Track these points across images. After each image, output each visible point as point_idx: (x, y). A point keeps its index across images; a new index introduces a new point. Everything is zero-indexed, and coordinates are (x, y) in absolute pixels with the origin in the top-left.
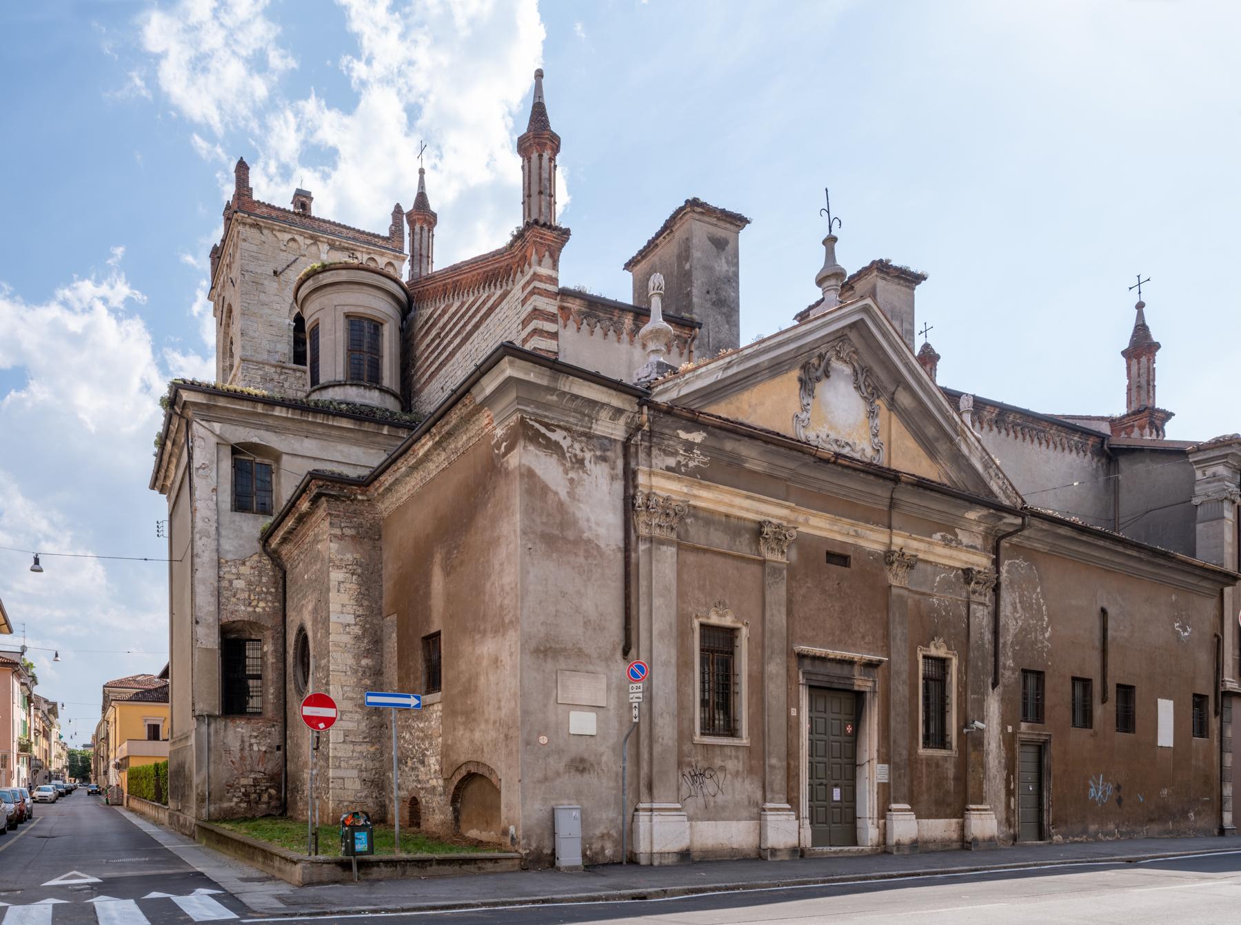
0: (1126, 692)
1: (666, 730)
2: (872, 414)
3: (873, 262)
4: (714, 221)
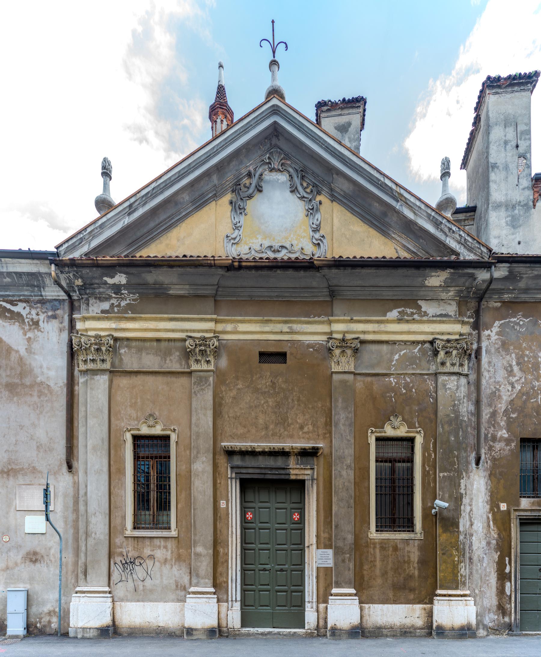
2: (312, 211)
3: (483, 84)
4: (339, 112)
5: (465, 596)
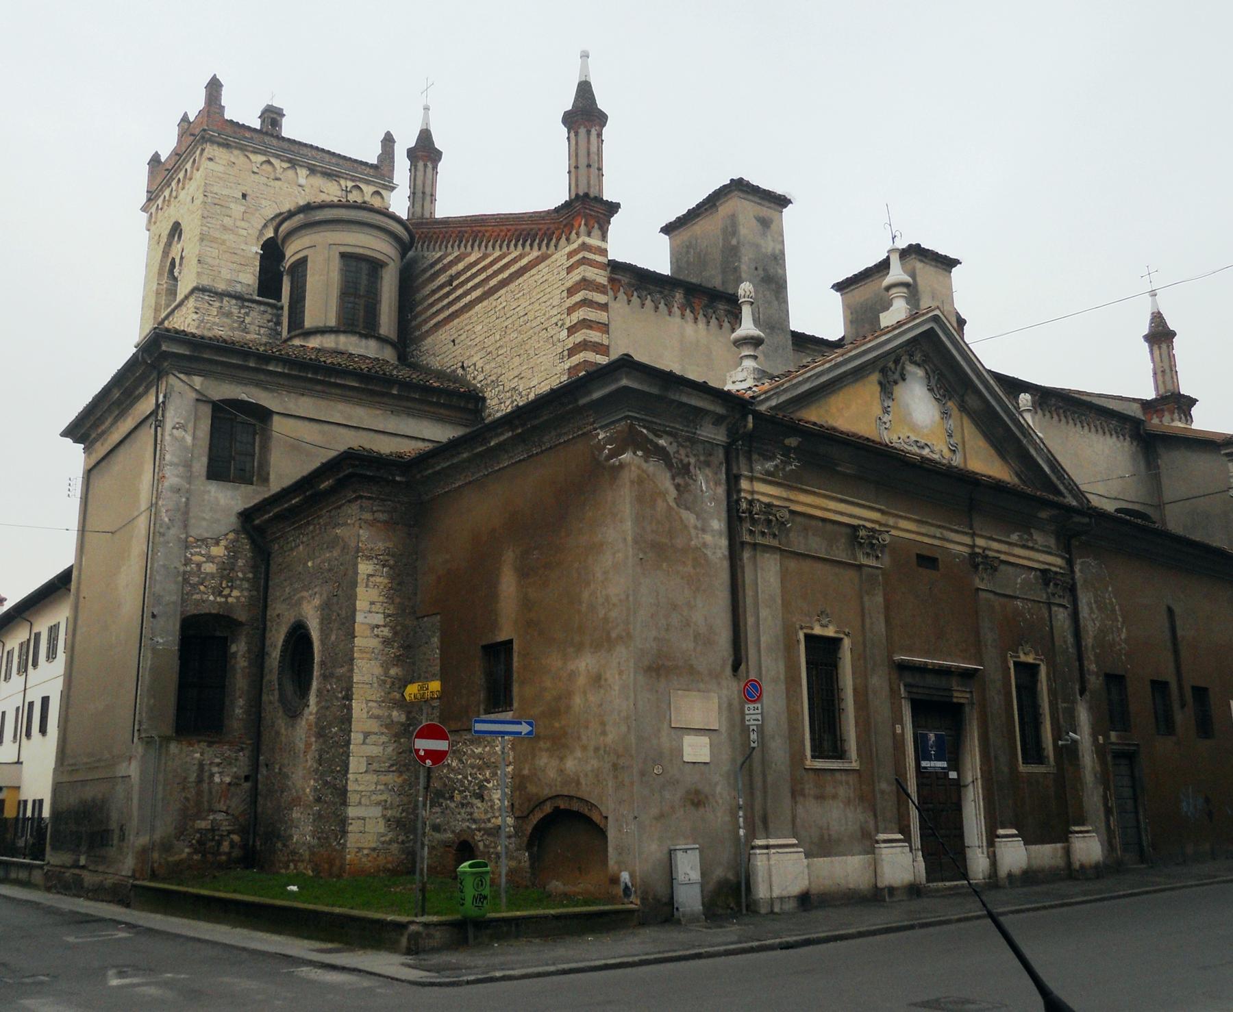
0: (1201, 693)
1: (779, 752)
5: (1087, 832)
